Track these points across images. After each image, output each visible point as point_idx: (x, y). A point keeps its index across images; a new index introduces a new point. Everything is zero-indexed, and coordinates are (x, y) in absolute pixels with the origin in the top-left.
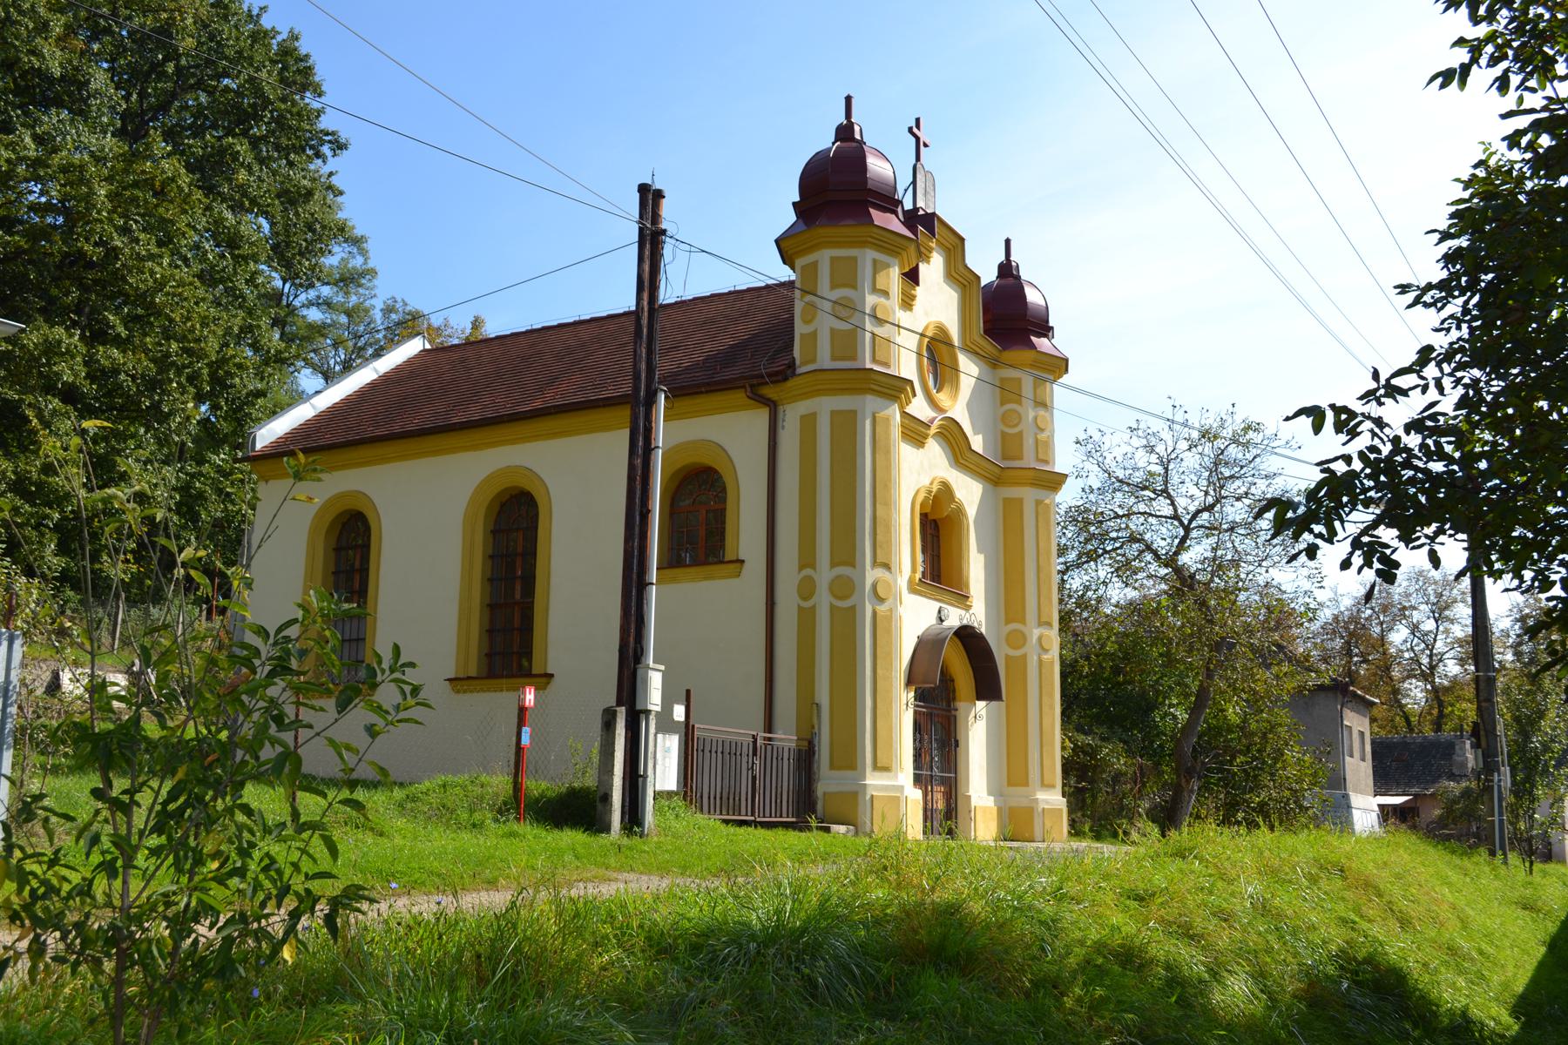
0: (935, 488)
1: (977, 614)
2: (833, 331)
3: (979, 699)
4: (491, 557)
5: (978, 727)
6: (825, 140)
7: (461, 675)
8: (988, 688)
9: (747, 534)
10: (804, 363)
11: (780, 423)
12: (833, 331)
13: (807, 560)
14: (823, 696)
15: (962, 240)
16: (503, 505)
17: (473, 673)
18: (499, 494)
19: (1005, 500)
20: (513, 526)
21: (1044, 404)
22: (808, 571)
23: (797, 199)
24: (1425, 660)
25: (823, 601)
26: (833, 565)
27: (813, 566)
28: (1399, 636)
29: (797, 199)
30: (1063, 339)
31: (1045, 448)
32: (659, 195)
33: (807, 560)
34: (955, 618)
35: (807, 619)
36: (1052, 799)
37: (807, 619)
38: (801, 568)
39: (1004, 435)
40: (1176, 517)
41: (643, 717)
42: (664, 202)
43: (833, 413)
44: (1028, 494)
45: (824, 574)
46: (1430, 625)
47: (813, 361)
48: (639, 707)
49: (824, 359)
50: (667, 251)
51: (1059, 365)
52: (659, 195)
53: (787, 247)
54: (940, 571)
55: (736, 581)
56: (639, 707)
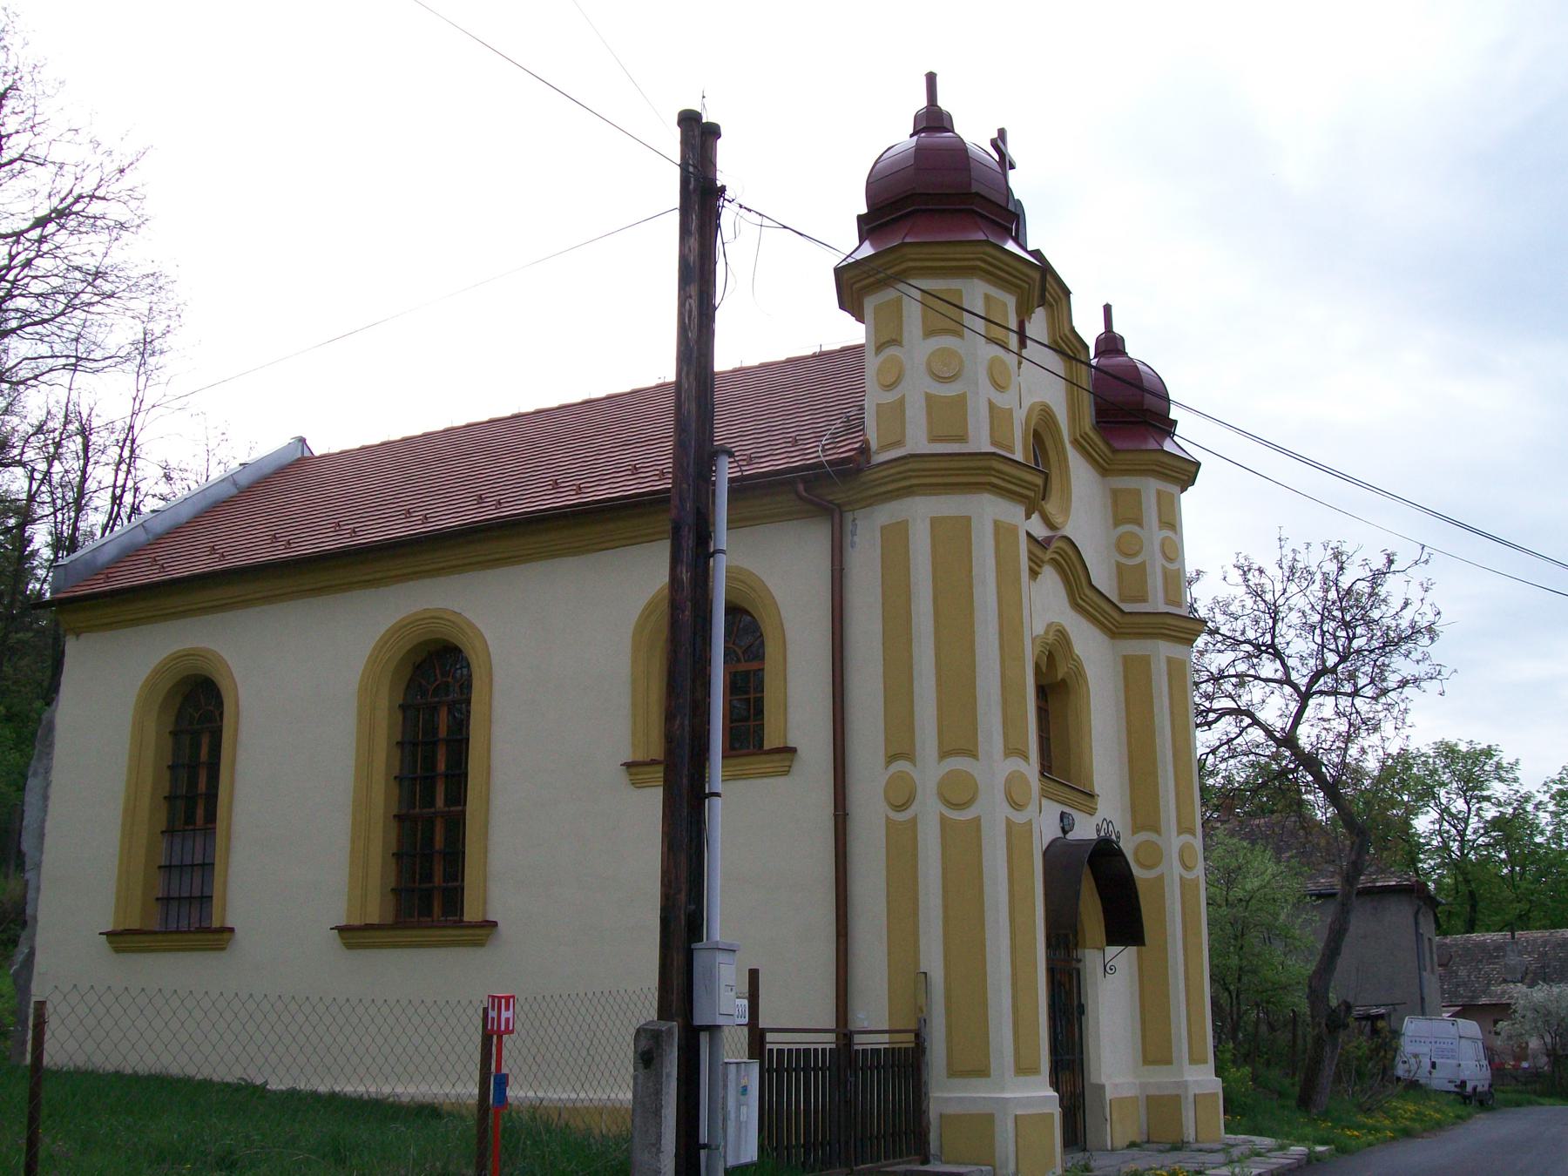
0: (1051, 638)
1: (1106, 815)
2: (929, 398)
3: (1110, 942)
4: (401, 744)
5: (1112, 982)
6: (898, 134)
7: (356, 922)
8: (1126, 924)
9: (799, 707)
10: (884, 448)
11: (847, 540)
12: (929, 398)
13: (900, 750)
14: (933, 960)
15: (1067, 293)
16: (418, 668)
17: (375, 920)
18: (414, 650)
19: (1125, 658)
20: (432, 704)
21: (1171, 522)
22: (901, 766)
23: (864, 210)
24: (1455, 846)
25: (929, 811)
26: (944, 754)
27: (908, 755)
28: (1423, 823)
29: (864, 210)
30: (1191, 433)
31: (1176, 581)
32: (713, 132)
33: (900, 750)
34: (1085, 829)
35: (902, 844)
36: (1202, 1079)
37: (902, 844)
38: (891, 759)
39: (1119, 566)
40: (1286, 680)
41: (704, 1038)
42: (722, 146)
43: (935, 522)
44: (1164, 650)
45: (929, 771)
46: (1459, 805)
47: (899, 443)
48: (700, 1019)
49: (918, 441)
50: (728, 216)
51: (1185, 472)
52: (713, 132)
53: (853, 286)
54: (1059, 763)
55: (780, 781)
56: (700, 1019)
